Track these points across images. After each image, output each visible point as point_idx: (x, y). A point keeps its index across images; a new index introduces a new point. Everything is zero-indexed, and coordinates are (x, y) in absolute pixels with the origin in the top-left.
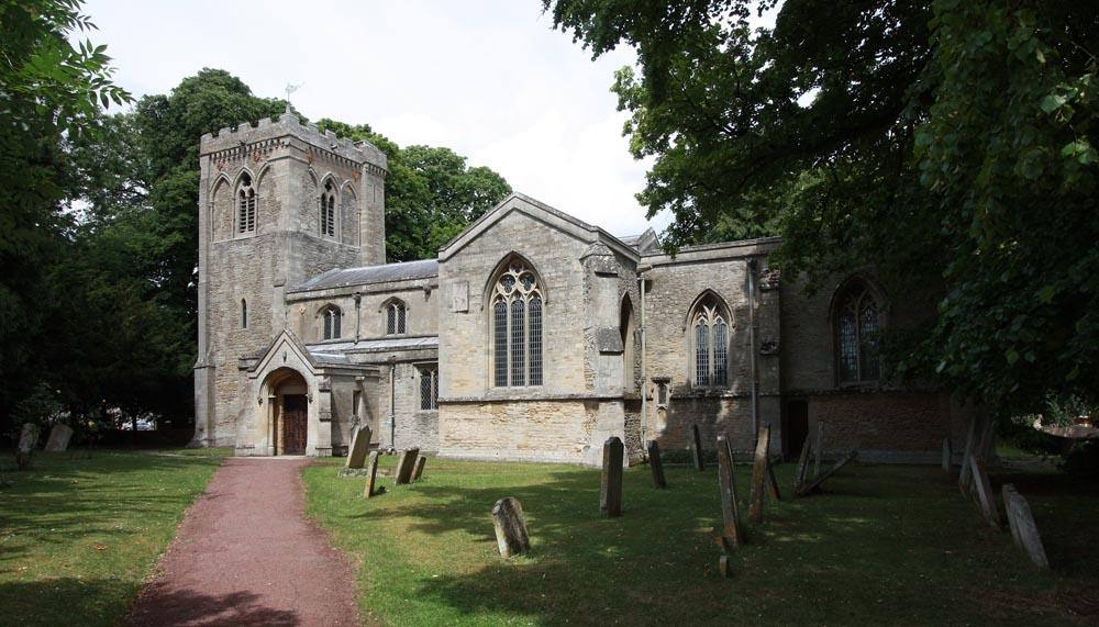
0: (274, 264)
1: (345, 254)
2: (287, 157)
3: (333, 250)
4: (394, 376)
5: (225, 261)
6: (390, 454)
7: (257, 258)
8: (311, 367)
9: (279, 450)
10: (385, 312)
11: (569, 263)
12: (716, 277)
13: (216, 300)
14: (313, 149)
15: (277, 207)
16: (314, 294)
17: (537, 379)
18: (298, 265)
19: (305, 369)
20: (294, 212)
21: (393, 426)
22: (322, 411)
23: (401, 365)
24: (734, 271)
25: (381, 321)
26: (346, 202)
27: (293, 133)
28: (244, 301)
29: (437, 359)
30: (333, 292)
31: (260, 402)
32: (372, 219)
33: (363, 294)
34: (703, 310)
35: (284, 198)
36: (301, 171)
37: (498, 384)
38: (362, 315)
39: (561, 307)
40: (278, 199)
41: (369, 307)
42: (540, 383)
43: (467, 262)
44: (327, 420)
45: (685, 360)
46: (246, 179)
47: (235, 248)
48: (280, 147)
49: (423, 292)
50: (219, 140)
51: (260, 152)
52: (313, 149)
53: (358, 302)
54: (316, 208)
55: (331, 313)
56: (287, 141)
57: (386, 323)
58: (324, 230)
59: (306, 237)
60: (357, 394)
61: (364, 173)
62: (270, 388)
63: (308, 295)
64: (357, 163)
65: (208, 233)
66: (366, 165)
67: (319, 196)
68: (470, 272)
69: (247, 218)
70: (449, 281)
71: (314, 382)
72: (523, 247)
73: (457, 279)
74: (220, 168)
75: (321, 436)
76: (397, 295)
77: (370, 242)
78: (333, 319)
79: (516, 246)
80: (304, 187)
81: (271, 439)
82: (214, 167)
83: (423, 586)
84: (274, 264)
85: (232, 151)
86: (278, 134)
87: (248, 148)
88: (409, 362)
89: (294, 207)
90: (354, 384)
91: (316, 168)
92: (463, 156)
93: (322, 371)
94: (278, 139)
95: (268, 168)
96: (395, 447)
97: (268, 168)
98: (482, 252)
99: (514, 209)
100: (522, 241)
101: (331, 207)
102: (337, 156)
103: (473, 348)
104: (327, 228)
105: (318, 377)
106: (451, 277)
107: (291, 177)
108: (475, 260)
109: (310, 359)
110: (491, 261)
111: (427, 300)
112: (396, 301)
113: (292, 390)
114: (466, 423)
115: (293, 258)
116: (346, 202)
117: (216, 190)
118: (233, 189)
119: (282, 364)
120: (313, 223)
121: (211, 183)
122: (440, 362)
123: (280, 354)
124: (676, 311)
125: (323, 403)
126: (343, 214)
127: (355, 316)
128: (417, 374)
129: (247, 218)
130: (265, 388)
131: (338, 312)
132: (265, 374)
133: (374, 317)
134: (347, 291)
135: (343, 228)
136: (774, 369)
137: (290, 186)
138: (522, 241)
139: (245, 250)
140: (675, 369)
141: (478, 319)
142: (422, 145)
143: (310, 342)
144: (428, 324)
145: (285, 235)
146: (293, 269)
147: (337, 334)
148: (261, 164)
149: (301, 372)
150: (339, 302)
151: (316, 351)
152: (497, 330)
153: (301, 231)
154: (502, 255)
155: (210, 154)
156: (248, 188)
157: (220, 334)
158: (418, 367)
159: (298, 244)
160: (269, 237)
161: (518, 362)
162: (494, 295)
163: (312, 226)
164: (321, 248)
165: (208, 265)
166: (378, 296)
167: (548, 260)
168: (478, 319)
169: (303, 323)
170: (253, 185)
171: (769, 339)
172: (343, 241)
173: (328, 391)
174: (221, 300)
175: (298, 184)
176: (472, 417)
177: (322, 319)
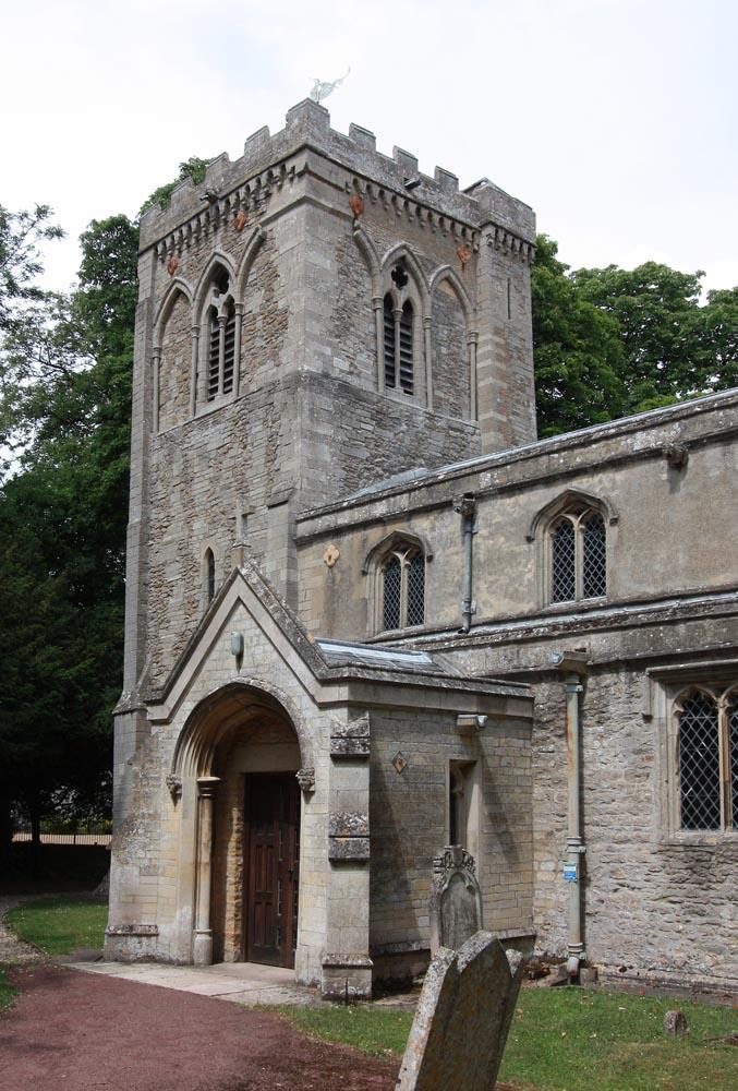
0: (271, 457)
1: (441, 436)
2: (299, 203)
3: (410, 421)
4: (581, 714)
5: (176, 469)
6: (575, 978)
7: (236, 450)
8: (308, 679)
9: (230, 946)
10: (545, 540)
13: (160, 559)
14: (363, 185)
16: (358, 515)
18: (326, 453)
19: (293, 686)
20: (316, 328)
21: (583, 880)
22: (340, 828)
23: (608, 679)
26: (443, 316)
27: (315, 144)
28: (210, 554)
30: (403, 502)
31: (176, 796)
32: (506, 354)
33: (481, 497)
35: (294, 297)
36: (338, 232)
38: (481, 556)
40: (281, 305)
41: (498, 529)
44: (357, 863)
47: (196, 438)
48: (287, 185)
49: (663, 463)
51: (247, 208)
52: (363, 185)
53: (469, 518)
54: (370, 324)
55: (402, 558)
56: (298, 163)
57: (548, 572)
58: (390, 379)
59: (345, 389)
60: (461, 772)
61: (484, 251)
63: (343, 519)
64: (466, 226)
65: (148, 414)
66: (490, 230)
67: (379, 294)
69: (222, 367)
71: (319, 726)
74: (172, 269)
75: (337, 921)
76: (580, 484)
77: (500, 409)
78: (404, 574)
80: (342, 272)
82: (162, 270)
83: (498, 848)
84: (271, 457)
87: (222, 206)
88: (634, 665)
89: (318, 318)
90: (454, 739)
91: (369, 230)
92: (692, 272)
93: (342, 693)
94: (281, 163)
95: (262, 241)
96: (592, 954)
101: (407, 326)
102: (420, 206)
104: (397, 372)
105: (333, 714)
107: (310, 246)
111: (673, 490)
112: (577, 502)
113: (264, 761)
115: (314, 437)
116: (443, 316)
117: (164, 323)
118: (200, 301)
119: (232, 675)
120: (362, 358)
121: (157, 307)
123: (227, 644)
125: (343, 802)
126: (436, 343)
127: (460, 560)
128: (665, 706)
129: (222, 367)
130: (188, 752)
131: (418, 555)
132: (188, 706)
133: (513, 556)
134: (440, 494)
135: (435, 376)
137: (309, 266)
139: (213, 437)
144: (682, 560)
145: (296, 381)
146: (313, 463)
147: (416, 614)
149: (282, 696)
150: (421, 527)
153: (335, 374)
155: (154, 246)
156: (223, 297)
157: (163, 635)
158: (669, 682)
159: (326, 402)
160: (262, 396)
163: (366, 373)
164: (381, 417)
165: (145, 484)
166: (523, 498)
169: (333, 593)
170: (233, 289)
172: (437, 407)
173: (359, 760)
174: (168, 557)
175: (327, 263)
177: (377, 579)
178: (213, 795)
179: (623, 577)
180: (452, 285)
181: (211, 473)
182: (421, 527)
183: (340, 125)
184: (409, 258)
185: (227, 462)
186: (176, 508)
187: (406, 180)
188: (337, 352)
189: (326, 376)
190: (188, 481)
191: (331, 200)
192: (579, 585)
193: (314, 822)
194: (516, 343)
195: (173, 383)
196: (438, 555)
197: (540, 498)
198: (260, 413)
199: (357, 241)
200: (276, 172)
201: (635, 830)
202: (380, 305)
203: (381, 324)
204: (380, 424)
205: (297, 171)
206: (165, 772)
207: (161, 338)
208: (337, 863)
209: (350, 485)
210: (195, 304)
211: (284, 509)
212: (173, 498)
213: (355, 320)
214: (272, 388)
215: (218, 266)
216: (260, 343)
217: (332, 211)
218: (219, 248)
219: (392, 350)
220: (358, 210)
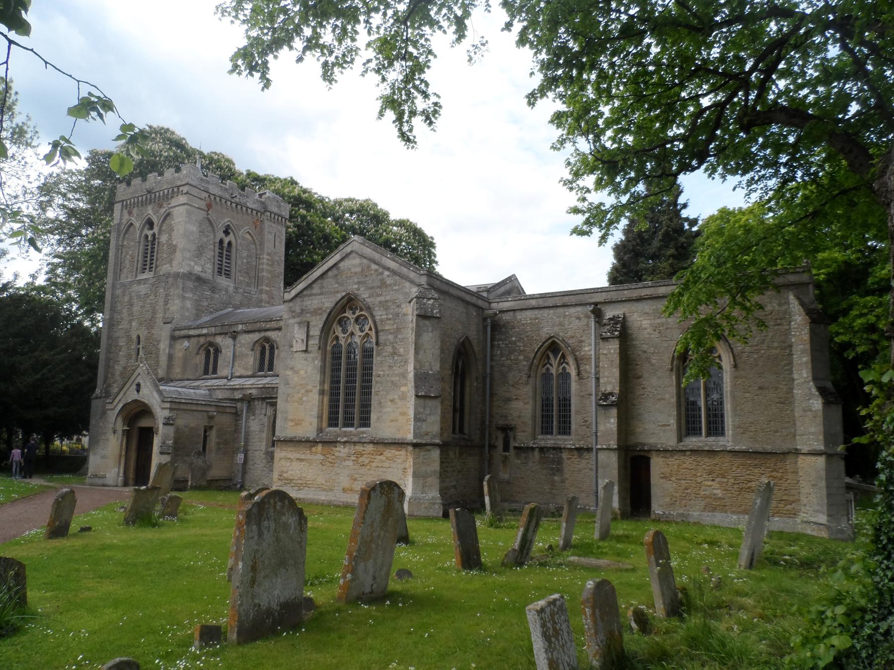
0: (166, 303)
2: (184, 204)
3: (227, 291)
5: (126, 299)
11: (399, 306)
12: (561, 324)
14: (212, 197)
15: (173, 249)
16: (197, 332)
17: (365, 422)
18: (188, 304)
20: (188, 255)
24: (579, 318)
25: (250, 360)
27: (191, 182)
28: (139, 337)
29: (276, 398)
30: (213, 330)
31: (114, 432)
34: (548, 358)
35: (179, 241)
37: (330, 425)
39: (389, 349)
42: (367, 425)
43: (309, 303)
45: (529, 407)
46: (150, 224)
47: (135, 288)
50: (131, 189)
52: (212, 197)
54: (211, 253)
56: (185, 189)
58: (220, 273)
62: (124, 420)
63: (192, 332)
68: (310, 313)
70: (292, 321)
71: (161, 413)
72: (358, 289)
73: (298, 320)
74: (130, 213)
76: (269, 334)
79: (352, 287)
80: (200, 232)
81: (122, 471)
82: (125, 212)
84: (166, 303)
85: (140, 199)
86: (179, 183)
89: (189, 251)
91: (213, 216)
94: (178, 187)
95: (168, 214)
97: (168, 214)
98: (321, 294)
99: (352, 252)
100: (359, 283)
101: (229, 251)
103: (309, 387)
104: (223, 270)
106: (294, 317)
108: (316, 302)
109: (160, 393)
110: (328, 303)
113: (144, 423)
114: (298, 463)
115: (184, 298)
117: (125, 234)
122: (279, 401)
124: (521, 357)
130: (120, 420)
132: (121, 405)
134: (225, 330)
136: (612, 420)
138: (359, 283)
139: (143, 289)
140: (520, 417)
141: (314, 359)
142: (313, 191)
143: (191, 377)
145: (177, 275)
147: (215, 371)
148: (163, 210)
149: (150, 404)
150: (219, 340)
151: (168, 389)
152: (333, 370)
154: (339, 296)
155: (123, 201)
156: (151, 232)
159: (190, 284)
161: (349, 405)
162: (331, 337)
163: (204, 267)
164: (214, 289)
167: (380, 302)
168: (314, 359)
169: (185, 360)
170: (156, 230)
171: (609, 389)
175: (194, 228)
176: (303, 457)
178: (127, 434)
180: (250, 234)
181: (141, 304)
182: (219, 340)
185: (148, 301)
188: (196, 264)
190: (131, 305)
191: (197, 203)
193: (157, 442)
194: (277, 258)
195: (127, 262)
196: (223, 351)
197: (256, 336)
198: (163, 284)
199: (209, 220)
200: (176, 190)
202: (217, 245)
203: (217, 250)
204: (213, 292)
206: (111, 426)
207: (123, 241)
208: (161, 453)
209: (198, 316)
210: (138, 232)
211: (169, 325)
212: (124, 311)
214: (168, 275)
215: (149, 219)
216: (165, 255)
218: (150, 211)
219: (221, 261)
220: (209, 206)
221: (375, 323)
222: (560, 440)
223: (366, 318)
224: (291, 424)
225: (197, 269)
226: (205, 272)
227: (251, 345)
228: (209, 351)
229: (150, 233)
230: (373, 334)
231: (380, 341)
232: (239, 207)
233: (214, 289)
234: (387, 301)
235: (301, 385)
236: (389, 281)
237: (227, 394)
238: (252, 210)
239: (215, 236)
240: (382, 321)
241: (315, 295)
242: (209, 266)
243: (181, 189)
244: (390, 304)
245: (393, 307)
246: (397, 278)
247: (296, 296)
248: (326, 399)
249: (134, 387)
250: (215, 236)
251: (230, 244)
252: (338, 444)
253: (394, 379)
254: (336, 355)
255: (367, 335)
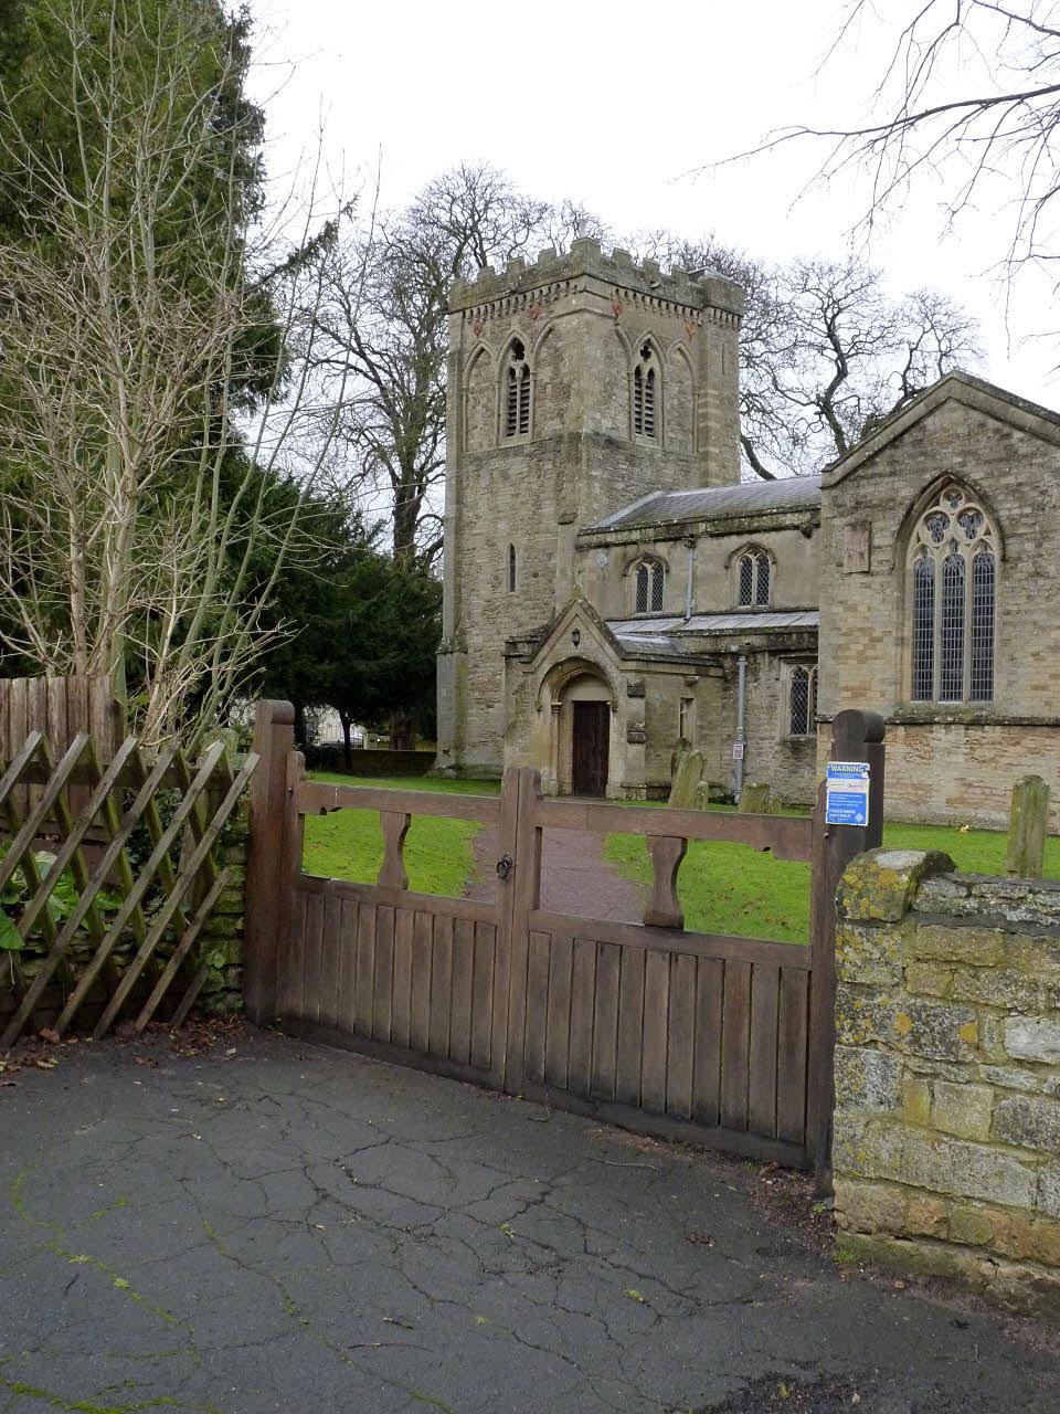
27: (589, 270)
43: (870, 489)
54: (623, 396)
63: (610, 538)
70: (838, 522)
72: (963, 464)
74: (478, 331)
76: (756, 538)
86: (567, 273)
98: (893, 474)
104: (644, 424)
105: (628, 675)
106: (842, 515)
113: (588, 693)
119: (574, 651)
130: (546, 692)
132: (546, 667)
147: (658, 604)
148: (539, 324)
149: (602, 664)
156: (520, 363)
162: (913, 545)
163: (614, 420)
166: (726, 540)
170: (528, 359)
179: (777, 596)
183: (606, 251)
184: (653, 339)
186: (482, 509)
187: (652, 282)
189: (597, 434)
192: (754, 597)
196: (673, 570)
197: (733, 542)
199: (617, 332)
201: (916, 995)
204: (632, 464)
205: (578, 289)
213: (615, 391)
217: (603, 316)
221: (998, 522)
222: (981, 709)
223: (978, 514)
224: (845, 694)
225: (606, 424)
226: (617, 429)
227: (724, 559)
228: (645, 569)
229: (518, 366)
230: (994, 540)
231: (1009, 554)
232: (664, 304)
233: (632, 460)
234: (1020, 484)
235: (861, 629)
236: (1023, 449)
237: (706, 645)
238: (685, 306)
239: (629, 364)
240: (1011, 519)
241: (881, 475)
242: (622, 420)
243: (573, 283)
244: (1026, 489)
245: (1033, 494)
246: (1039, 442)
247: (845, 478)
248: (908, 653)
249: (568, 635)
250: (629, 364)
251: (651, 373)
252: (935, 727)
253: (1035, 617)
254: (924, 582)
255: (985, 545)
